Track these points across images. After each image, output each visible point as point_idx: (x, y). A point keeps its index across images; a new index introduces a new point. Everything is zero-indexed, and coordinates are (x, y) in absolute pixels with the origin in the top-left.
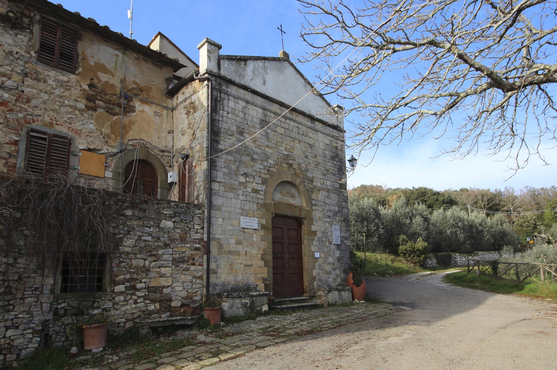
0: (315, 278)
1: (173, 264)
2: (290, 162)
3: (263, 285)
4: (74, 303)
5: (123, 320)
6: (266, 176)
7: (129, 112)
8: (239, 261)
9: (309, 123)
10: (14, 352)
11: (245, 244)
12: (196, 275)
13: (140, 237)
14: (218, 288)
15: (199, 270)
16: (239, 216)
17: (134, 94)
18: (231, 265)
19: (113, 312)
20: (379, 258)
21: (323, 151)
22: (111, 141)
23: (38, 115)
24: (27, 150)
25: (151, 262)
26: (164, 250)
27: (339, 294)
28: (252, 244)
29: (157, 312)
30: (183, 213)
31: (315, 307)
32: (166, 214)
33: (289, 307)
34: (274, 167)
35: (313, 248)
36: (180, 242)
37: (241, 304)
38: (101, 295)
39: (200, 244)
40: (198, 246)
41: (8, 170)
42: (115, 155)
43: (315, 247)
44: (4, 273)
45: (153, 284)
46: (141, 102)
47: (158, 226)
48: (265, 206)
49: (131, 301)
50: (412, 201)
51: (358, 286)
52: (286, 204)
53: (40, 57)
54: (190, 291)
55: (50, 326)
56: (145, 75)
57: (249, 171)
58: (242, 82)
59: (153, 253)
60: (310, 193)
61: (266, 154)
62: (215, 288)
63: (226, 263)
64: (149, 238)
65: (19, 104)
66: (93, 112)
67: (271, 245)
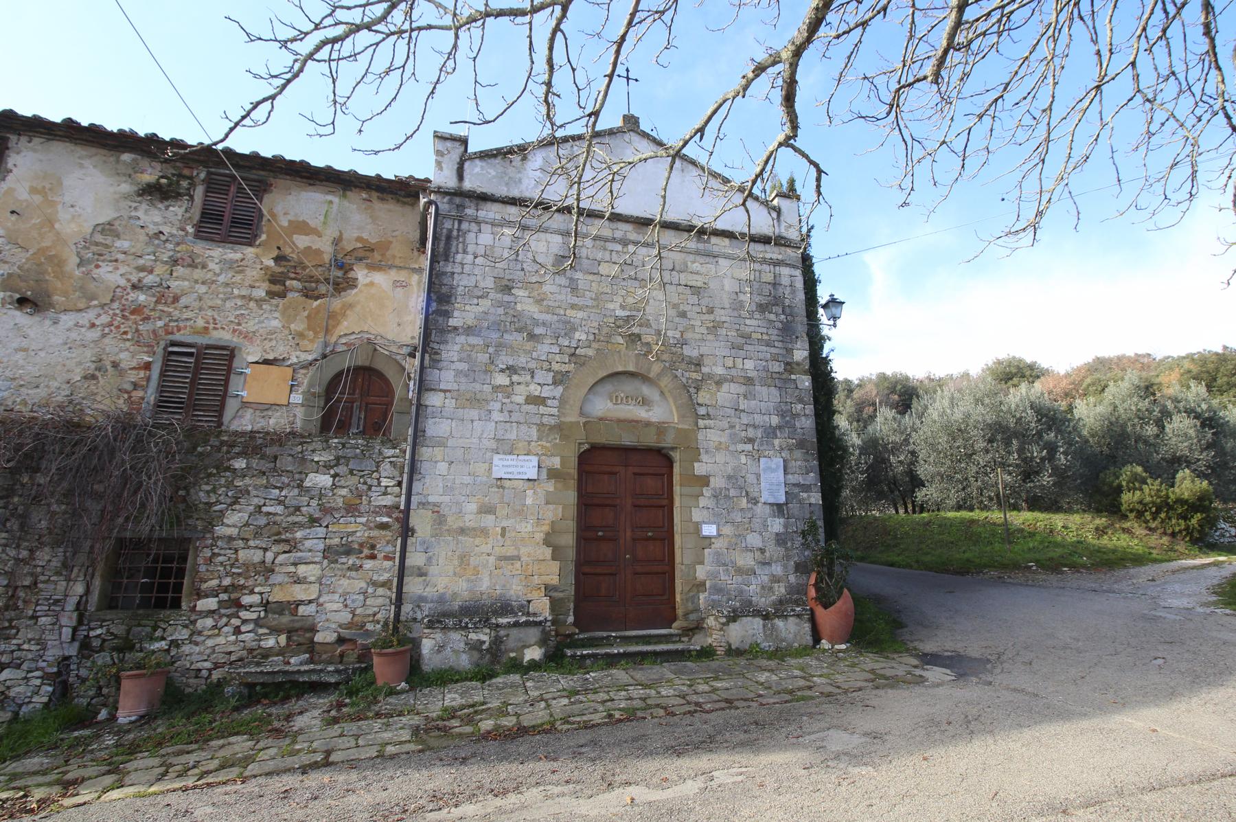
0: (703, 584)
2: (636, 330)
3: (546, 601)
4: (119, 629)
5: (208, 665)
6: (565, 368)
7: (344, 290)
8: (486, 548)
9: (692, 245)
10: (8, 709)
11: (502, 511)
12: (375, 578)
13: (260, 507)
15: (384, 570)
16: (489, 454)
17: (356, 259)
18: (464, 559)
19: (186, 649)
20: (1060, 524)
21: (735, 297)
22: (306, 342)
23: (187, 319)
24: (163, 374)
25: (277, 555)
26: (308, 531)
27: (764, 626)
28: (521, 513)
29: (281, 652)
30: (356, 457)
31: (706, 653)
32: (317, 462)
33: (598, 654)
34: (590, 347)
35: (697, 515)
36: (343, 512)
37: (466, 644)
38: (169, 615)
39: (390, 517)
40: (385, 519)
43: (705, 512)
44: (10, 575)
45: (278, 596)
47: (300, 486)
48: (561, 430)
49: (226, 629)
50: (1225, 379)
52: (619, 421)
53: (199, 231)
54: (358, 611)
55: (72, 667)
57: (522, 361)
58: (515, 193)
59: (283, 537)
60: (692, 390)
61: (570, 322)
62: (419, 606)
63: (450, 553)
64: (279, 509)
65: (160, 307)
66: (279, 300)
67: (572, 512)
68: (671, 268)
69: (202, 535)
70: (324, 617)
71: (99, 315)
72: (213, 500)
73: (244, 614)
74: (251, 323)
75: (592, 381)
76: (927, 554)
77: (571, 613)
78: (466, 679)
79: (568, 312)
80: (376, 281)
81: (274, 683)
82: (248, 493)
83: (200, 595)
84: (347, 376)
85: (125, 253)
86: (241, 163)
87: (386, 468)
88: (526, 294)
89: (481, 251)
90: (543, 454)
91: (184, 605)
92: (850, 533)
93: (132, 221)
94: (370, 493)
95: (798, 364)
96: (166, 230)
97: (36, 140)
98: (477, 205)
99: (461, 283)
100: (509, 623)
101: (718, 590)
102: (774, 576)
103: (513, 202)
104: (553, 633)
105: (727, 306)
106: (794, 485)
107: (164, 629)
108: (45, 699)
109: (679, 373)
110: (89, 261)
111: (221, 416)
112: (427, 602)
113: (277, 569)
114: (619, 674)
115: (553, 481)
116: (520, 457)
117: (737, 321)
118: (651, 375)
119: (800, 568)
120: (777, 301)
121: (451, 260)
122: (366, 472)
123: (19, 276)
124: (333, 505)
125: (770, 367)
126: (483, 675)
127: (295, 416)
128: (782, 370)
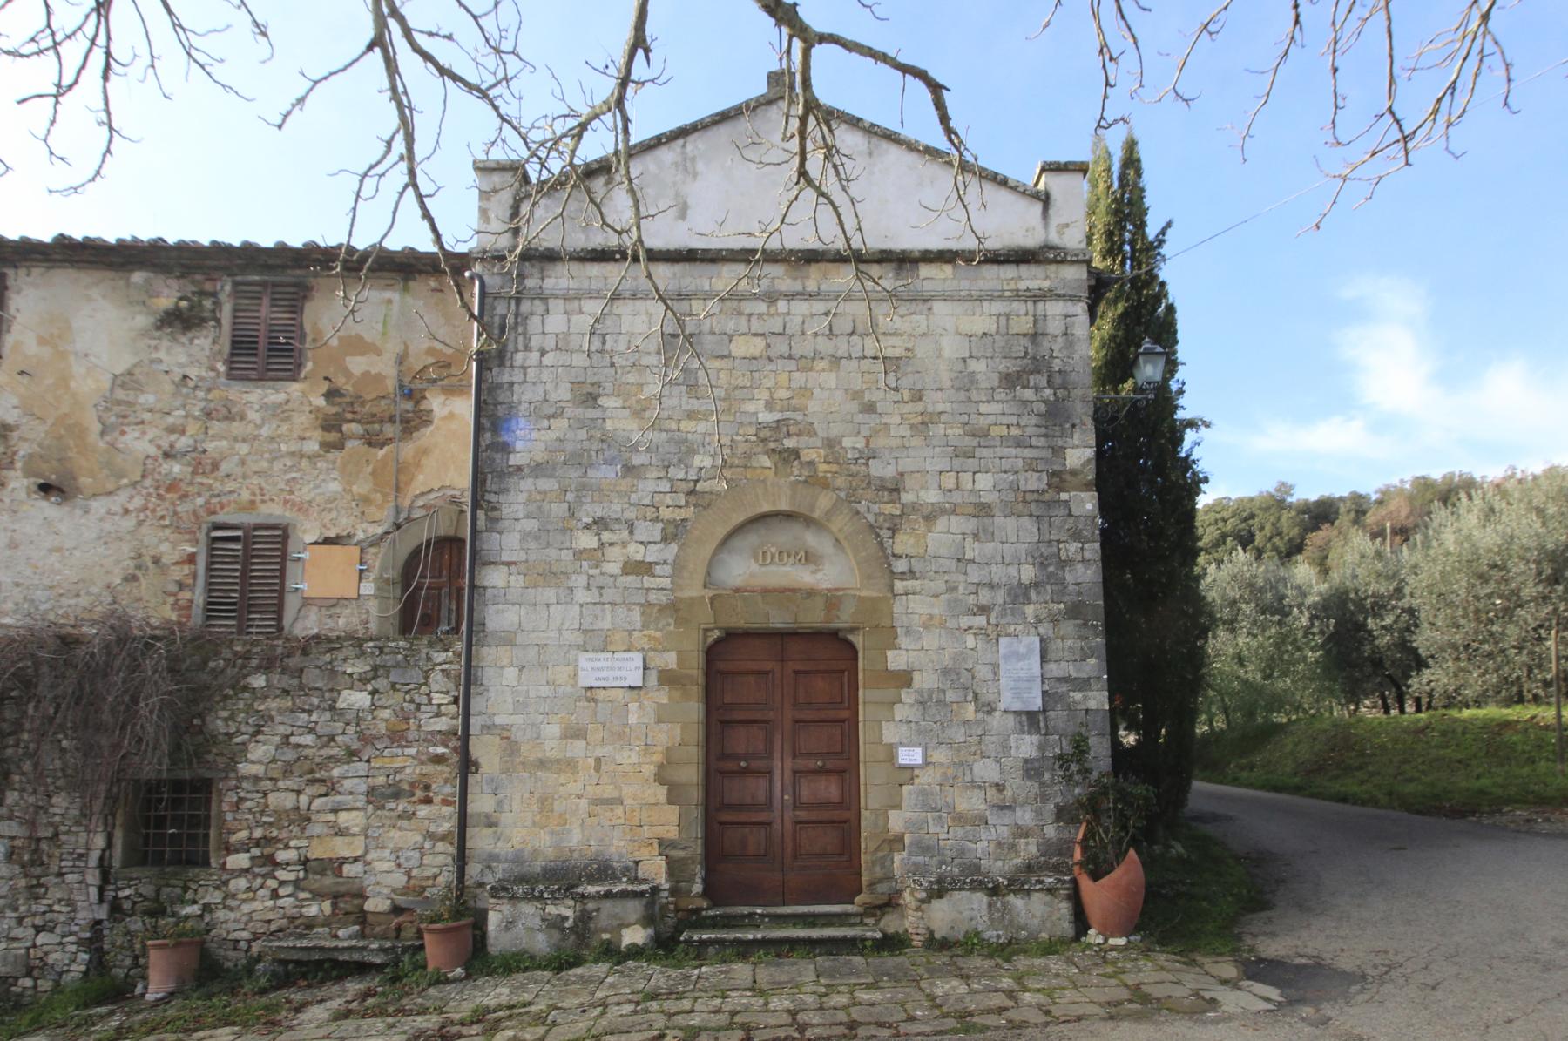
1: (369, 802)
2: (789, 443)
3: (661, 861)
4: (147, 890)
5: (246, 935)
6: (680, 514)
7: (417, 428)
8: (575, 788)
11: (595, 735)
12: (432, 829)
13: (287, 737)
14: (501, 866)
16: (573, 652)
18: (545, 803)
19: (221, 915)
21: (960, 366)
22: (373, 509)
23: (231, 492)
24: (209, 569)
25: (313, 798)
26: (346, 767)
27: (990, 905)
28: (622, 737)
30: (397, 665)
32: (351, 675)
35: (890, 734)
36: (387, 742)
37: (543, 920)
38: (198, 875)
39: (446, 746)
40: (440, 750)
41: (179, 616)
42: (382, 538)
43: (904, 728)
45: (317, 851)
46: (444, 394)
47: (332, 708)
49: (261, 892)
52: (766, 592)
57: (615, 509)
59: (318, 776)
60: (885, 533)
61: (686, 440)
62: (489, 867)
63: (527, 795)
64: (308, 739)
65: (199, 479)
67: (696, 733)
68: (849, 331)
69: (223, 775)
70: (373, 879)
71: (132, 497)
72: (232, 730)
73: (282, 875)
74: (305, 489)
75: (721, 532)
76: (1411, 780)
77: (698, 880)
78: (540, 967)
79: (683, 425)
80: (457, 411)
81: (309, 961)
82: (271, 718)
83: (229, 849)
84: (427, 555)
85: (150, 411)
86: (270, 262)
87: (437, 679)
88: (619, 403)
89: (550, 343)
90: (651, 649)
91: (214, 862)
92: (1289, 748)
93: (155, 366)
94: (419, 715)
95: (1074, 473)
96: (193, 372)
97: (36, 271)
98: (542, 270)
99: (524, 398)
100: (598, 892)
101: (924, 849)
102: (1019, 827)
103: (602, 256)
104: (672, 907)
105: (947, 384)
106: (1059, 680)
107: (196, 891)
108: (83, 968)
109: (862, 507)
110: (113, 427)
111: (280, 618)
112: (499, 861)
113: (313, 817)
114: (741, 971)
115: (667, 687)
116: (616, 655)
117: (963, 408)
118: (817, 514)
119: (1063, 815)
120: (1038, 364)
121: (508, 363)
122: (412, 686)
123: (41, 457)
124: (374, 732)
125: (1022, 483)
126: (560, 963)
127: (368, 612)
128: (1043, 485)
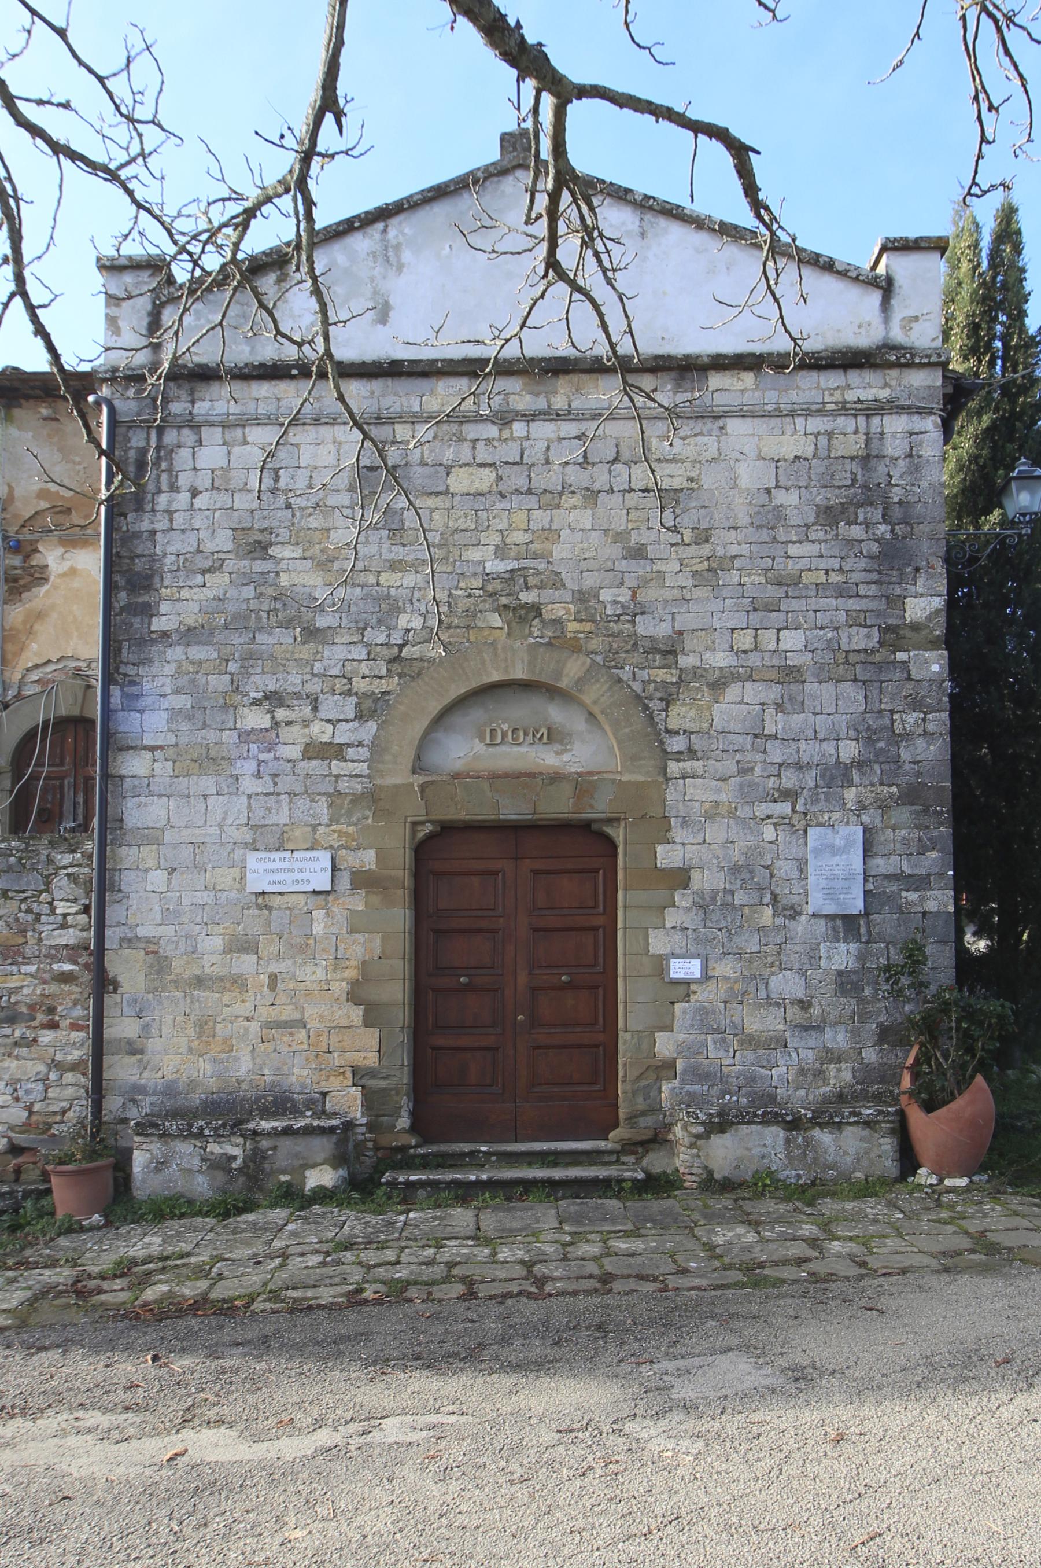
3: (356, 1093)
12: (59, 1057)
21: (764, 498)
27: (788, 1141)
37: (203, 1160)
39: (76, 963)
40: (67, 967)
46: (64, 546)
48: (375, 801)
51: (929, 1107)
56: (77, 459)
63: (179, 1018)
